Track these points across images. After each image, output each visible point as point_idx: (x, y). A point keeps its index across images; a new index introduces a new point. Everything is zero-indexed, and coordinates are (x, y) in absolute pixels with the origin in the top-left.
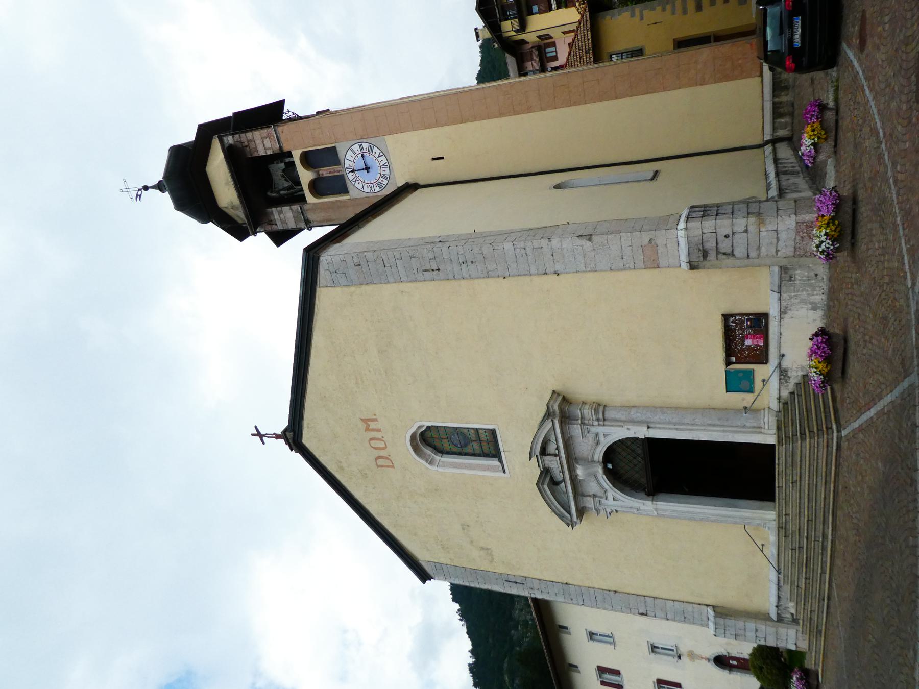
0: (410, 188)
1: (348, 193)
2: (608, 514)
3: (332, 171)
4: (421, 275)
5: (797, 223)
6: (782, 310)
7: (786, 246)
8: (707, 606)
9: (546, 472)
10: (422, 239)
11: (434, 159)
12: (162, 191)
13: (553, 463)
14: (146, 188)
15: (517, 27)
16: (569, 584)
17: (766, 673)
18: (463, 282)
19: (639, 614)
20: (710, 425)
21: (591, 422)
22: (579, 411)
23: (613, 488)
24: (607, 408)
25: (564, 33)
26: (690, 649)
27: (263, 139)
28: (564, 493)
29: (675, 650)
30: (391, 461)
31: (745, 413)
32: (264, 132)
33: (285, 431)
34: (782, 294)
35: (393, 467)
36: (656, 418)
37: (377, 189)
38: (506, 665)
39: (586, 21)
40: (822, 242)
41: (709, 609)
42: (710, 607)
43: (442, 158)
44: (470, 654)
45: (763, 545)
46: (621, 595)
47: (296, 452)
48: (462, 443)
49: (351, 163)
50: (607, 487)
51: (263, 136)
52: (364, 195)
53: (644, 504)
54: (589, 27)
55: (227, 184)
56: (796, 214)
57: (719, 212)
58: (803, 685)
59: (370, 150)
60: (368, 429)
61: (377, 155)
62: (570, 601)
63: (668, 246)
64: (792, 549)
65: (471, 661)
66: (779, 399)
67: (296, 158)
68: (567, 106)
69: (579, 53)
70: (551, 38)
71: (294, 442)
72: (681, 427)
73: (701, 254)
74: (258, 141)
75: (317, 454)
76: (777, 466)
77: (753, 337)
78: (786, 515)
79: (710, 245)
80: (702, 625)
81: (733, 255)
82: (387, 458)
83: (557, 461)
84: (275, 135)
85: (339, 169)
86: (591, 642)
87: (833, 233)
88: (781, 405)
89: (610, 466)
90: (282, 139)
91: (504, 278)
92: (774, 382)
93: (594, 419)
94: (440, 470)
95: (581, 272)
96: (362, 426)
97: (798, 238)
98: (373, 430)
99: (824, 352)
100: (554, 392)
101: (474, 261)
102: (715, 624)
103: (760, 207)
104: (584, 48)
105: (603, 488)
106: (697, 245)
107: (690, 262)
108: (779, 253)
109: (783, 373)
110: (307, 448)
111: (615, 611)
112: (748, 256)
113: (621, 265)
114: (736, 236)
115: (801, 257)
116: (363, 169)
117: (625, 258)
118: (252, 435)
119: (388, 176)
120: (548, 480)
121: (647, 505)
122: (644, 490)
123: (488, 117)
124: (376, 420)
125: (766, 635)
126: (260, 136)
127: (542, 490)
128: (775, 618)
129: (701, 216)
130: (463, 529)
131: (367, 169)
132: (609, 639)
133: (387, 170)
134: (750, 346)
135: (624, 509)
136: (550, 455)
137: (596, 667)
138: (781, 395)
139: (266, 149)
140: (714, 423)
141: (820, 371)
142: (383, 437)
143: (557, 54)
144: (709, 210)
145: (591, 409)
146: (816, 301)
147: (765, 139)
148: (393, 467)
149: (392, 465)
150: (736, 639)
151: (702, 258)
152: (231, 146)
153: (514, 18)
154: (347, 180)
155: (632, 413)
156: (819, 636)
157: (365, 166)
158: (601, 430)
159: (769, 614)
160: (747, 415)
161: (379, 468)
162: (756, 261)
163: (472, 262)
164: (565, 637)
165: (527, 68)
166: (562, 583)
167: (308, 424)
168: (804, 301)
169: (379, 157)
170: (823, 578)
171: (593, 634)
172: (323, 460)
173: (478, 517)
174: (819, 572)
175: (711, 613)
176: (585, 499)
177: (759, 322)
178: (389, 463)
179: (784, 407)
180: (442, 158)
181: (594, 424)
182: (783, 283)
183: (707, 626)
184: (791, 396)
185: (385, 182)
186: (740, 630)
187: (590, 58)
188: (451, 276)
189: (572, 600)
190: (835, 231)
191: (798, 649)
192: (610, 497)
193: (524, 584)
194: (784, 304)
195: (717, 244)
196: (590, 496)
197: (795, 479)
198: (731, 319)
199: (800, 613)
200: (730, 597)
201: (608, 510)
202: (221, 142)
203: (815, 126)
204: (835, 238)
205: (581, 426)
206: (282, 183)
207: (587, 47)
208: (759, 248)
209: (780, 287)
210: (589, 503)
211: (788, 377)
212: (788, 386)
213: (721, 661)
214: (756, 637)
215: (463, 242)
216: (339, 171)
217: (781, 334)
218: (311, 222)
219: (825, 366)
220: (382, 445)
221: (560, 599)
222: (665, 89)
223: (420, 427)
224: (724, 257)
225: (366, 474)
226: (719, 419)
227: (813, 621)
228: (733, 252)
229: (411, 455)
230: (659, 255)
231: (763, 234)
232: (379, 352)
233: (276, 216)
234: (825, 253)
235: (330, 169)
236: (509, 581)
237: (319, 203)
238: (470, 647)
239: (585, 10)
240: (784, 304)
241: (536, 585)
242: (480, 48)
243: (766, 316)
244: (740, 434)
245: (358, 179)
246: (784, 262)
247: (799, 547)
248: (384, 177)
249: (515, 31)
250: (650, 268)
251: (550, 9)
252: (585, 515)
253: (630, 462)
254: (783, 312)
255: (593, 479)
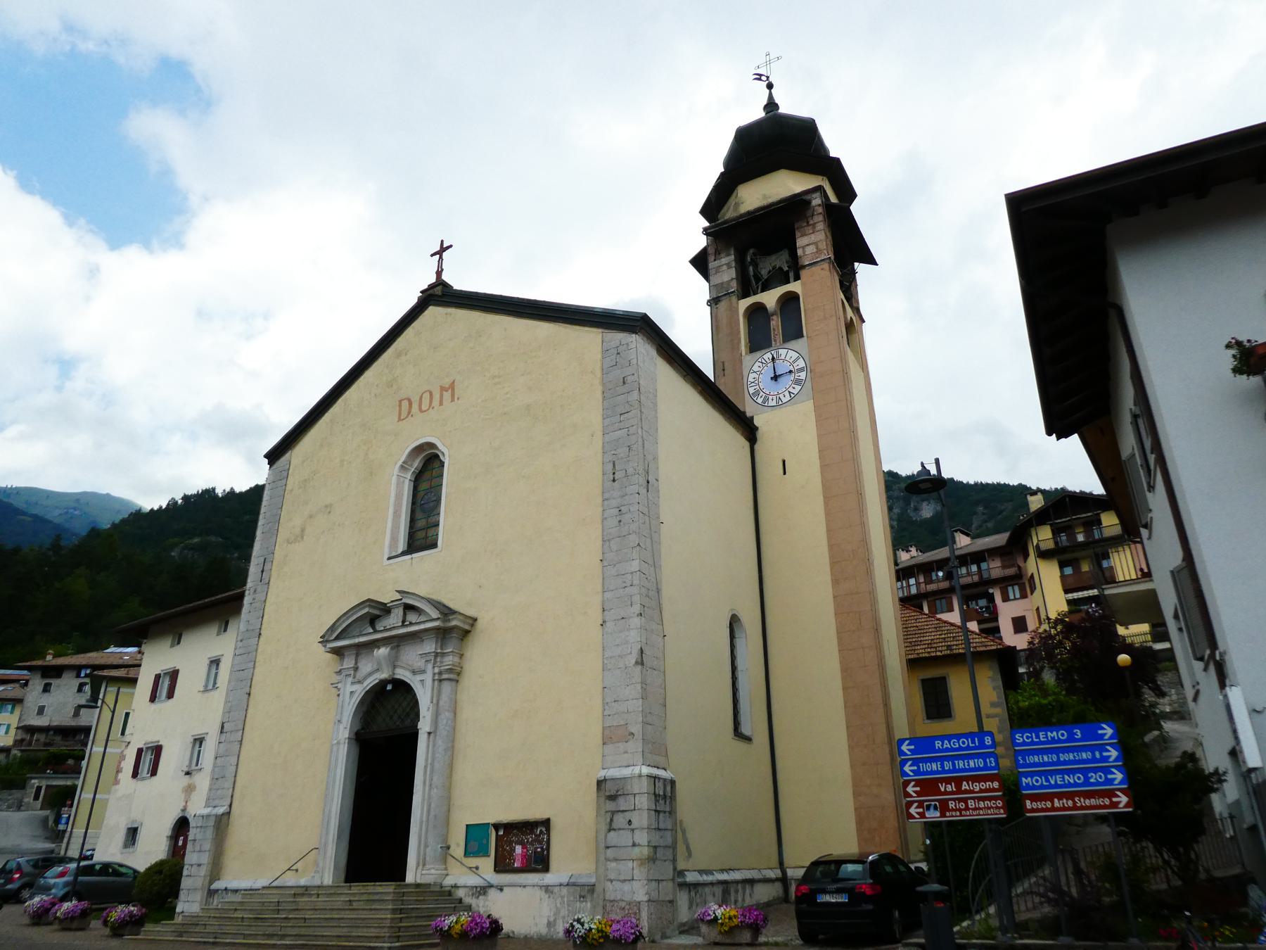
0: (748, 429)
1: (750, 353)
2: (336, 685)
3: (776, 333)
4: (610, 459)
5: (639, 903)
6: (549, 888)
7: (616, 891)
8: (230, 806)
9: (386, 610)
10: (655, 459)
11: (784, 462)
12: (766, 107)
13: (395, 618)
14: (770, 86)
15: (1044, 546)
16: (259, 637)
17: (154, 878)
18: (600, 509)
19: (223, 723)
20: (429, 805)
21: (438, 664)
22: (451, 650)
23: (365, 691)
24: (454, 683)
25: (1038, 609)
26: (197, 789)
27: (816, 244)
28: (361, 631)
29: (197, 768)
30: (407, 417)
31: (441, 847)
32: (823, 246)
33: (445, 285)
34: (566, 888)
35: (400, 420)
36: (440, 742)
37: (752, 390)
38: (213, 539)
39: (986, 646)
40: (582, 925)
41: (225, 808)
42: (229, 809)
43: (785, 473)
44: (228, 490)
45: (297, 870)
46: (246, 701)
47: (419, 298)
48: (426, 506)
49: (783, 357)
50: (365, 684)
51: (819, 244)
52: (745, 374)
53: (346, 728)
54: (978, 649)
55: (765, 197)
56: (649, 901)
57: (661, 815)
58: (124, 918)
59: (798, 382)
60: (443, 389)
61: (791, 390)
62: (239, 639)
63: (626, 755)
64: (278, 902)
65: (219, 492)
66: (456, 886)
67: (794, 287)
68: (837, 627)
69: (950, 637)
70: (1032, 593)
71: (430, 295)
72: (428, 773)
73: (613, 793)
74: (813, 238)
75: (416, 324)
76: (373, 883)
77: (524, 856)
78: (318, 895)
79: (622, 804)
80: (208, 799)
81: (610, 830)
82: (409, 413)
83: (397, 623)
84: (819, 259)
85: (778, 341)
86: (208, 662)
87: (591, 936)
88: (449, 888)
89: (389, 687)
90: (814, 269)
91: (601, 560)
92: (473, 880)
93: (442, 668)
94: (394, 479)
95: (603, 653)
96: (446, 382)
97: (623, 904)
98: (441, 396)
99: (471, 930)
100: (475, 620)
101: (622, 523)
102: (208, 816)
103: (665, 861)
104: (955, 643)
105: (365, 678)
106: (623, 789)
107: (605, 780)
108: (609, 883)
109: (482, 890)
110: (423, 312)
111: (227, 694)
112: (608, 847)
113: (608, 700)
114: (629, 833)
115: (604, 908)
116: (775, 373)
117: (615, 705)
118: (442, 241)
119: (766, 404)
120: (376, 612)
121: (344, 733)
122: (362, 729)
123: (830, 531)
124: (453, 400)
125: (194, 876)
126: (819, 240)
127: (362, 606)
128: (213, 887)
129: (657, 792)
130: (326, 506)
131: (776, 378)
132: (211, 685)
133: (774, 403)
134: (515, 852)
135: (340, 703)
136: (405, 614)
137: (177, 668)
138: (460, 889)
139: (803, 248)
140: (432, 810)
141: (453, 926)
142: (433, 408)
143: (1012, 600)
144: (666, 801)
145: (453, 665)
146: (557, 927)
147: (788, 870)
148: (400, 420)
149: (402, 418)
150: (17, 728)
151: (608, 794)
152: (809, 202)
153: (1056, 543)
154: (764, 351)
155: (447, 714)
156: (176, 934)
157: (779, 375)
158: (428, 677)
159: (219, 879)
160: (440, 850)
161: (398, 402)
162: (602, 858)
163: (620, 521)
164: (213, 629)
165: (993, 560)
166: (260, 629)
167: (451, 314)
168: (557, 913)
169: (789, 392)
170: (239, 936)
171: (218, 665)
172: (409, 332)
173: (339, 525)
174: (246, 932)
175: (221, 810)
176: (353, 657)
177: (540, 862)
178: (404, 415)
179: (444, 892)
180: (785, 473)
181: (436, 668)
182: (578, 888)
183: (207, 806)
184: (457, 899)
185: (760, 401)
186: (200, 846)
187: (941, 651)
188: (607, 496)
189: (241, 641)
190: (593, 939)
191: (176, 916)
192: (354, 688)
193: (261, 581)
194: (556, 890)
195: (623, 811)
196: (356, 663)
197: (354, 904)
198: (544, 829)
199: (207, 912)
200: (239, 833)
201: (339, 685)
202: (819, 189)
203: (735, 920)
204: (586, 939)
205: (434, 652)
206: (766, 267)
207: (955, 647)
208: (616, 860)
209: (574, 885)
210: (349, 662)
211: (478, 897)
212: (469, 896)
213: (182, 825)
214: (192, 865)
215: (646, 510)
216: (775, 341)
217: (525, 886)
218: (716, 304)
219: (457, 931)
220: (424, 408)
221: (243, 626)
222: (851, 748)
223: (443, 454)
224: (608, 820)
225: (392, 386)
226: (435, 816)
227: (194, 927)
228: (614, 830)
229: (413, 443)
230: (617, 745)
231: (630, 864)
232: (528, 406)
233: (724, 260)
234: (570, 929)
235: (778, 329)
236: (264, 563)
237: (738, 316)
238: (237, 490)
239: (1000, 644)
240: (556, 890)
241: (260, 597)
242: (1062, 489)
243: (546, 869)
244: (417, 842)
245: (764, 365)
246: (599, 889)
247: (279, 910)
248: (766, 400)
249: (1038, 545)
250: (603, 734)
251: (1066, 591)
252: (335, 656)
253: (395, 712)
254: (547, 889)
255: (375, 667)
